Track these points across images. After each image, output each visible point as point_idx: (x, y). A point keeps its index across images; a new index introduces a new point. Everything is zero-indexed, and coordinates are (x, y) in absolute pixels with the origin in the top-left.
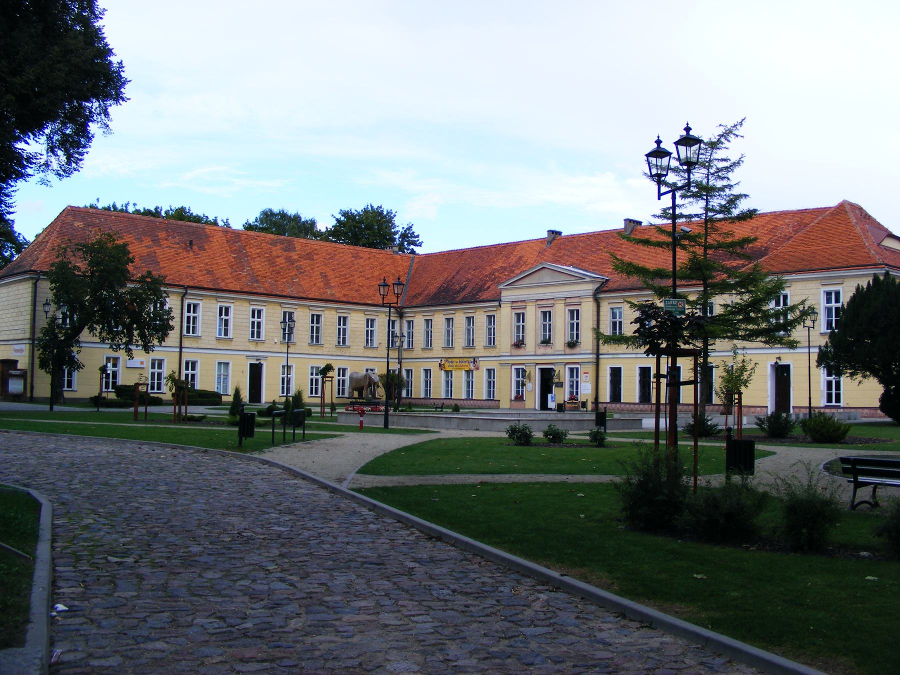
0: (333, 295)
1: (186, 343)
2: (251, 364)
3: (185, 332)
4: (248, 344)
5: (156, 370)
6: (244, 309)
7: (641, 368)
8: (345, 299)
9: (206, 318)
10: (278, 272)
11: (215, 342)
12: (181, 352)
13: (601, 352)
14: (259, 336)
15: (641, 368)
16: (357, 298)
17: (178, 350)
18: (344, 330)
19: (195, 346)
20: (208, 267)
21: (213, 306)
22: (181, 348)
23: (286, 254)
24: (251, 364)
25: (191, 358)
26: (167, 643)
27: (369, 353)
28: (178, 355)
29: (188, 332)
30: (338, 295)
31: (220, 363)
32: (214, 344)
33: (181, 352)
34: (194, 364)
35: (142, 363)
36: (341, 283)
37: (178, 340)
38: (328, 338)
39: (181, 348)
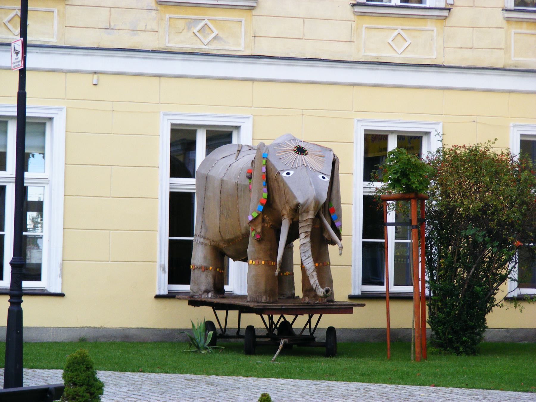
26: (373, 209)
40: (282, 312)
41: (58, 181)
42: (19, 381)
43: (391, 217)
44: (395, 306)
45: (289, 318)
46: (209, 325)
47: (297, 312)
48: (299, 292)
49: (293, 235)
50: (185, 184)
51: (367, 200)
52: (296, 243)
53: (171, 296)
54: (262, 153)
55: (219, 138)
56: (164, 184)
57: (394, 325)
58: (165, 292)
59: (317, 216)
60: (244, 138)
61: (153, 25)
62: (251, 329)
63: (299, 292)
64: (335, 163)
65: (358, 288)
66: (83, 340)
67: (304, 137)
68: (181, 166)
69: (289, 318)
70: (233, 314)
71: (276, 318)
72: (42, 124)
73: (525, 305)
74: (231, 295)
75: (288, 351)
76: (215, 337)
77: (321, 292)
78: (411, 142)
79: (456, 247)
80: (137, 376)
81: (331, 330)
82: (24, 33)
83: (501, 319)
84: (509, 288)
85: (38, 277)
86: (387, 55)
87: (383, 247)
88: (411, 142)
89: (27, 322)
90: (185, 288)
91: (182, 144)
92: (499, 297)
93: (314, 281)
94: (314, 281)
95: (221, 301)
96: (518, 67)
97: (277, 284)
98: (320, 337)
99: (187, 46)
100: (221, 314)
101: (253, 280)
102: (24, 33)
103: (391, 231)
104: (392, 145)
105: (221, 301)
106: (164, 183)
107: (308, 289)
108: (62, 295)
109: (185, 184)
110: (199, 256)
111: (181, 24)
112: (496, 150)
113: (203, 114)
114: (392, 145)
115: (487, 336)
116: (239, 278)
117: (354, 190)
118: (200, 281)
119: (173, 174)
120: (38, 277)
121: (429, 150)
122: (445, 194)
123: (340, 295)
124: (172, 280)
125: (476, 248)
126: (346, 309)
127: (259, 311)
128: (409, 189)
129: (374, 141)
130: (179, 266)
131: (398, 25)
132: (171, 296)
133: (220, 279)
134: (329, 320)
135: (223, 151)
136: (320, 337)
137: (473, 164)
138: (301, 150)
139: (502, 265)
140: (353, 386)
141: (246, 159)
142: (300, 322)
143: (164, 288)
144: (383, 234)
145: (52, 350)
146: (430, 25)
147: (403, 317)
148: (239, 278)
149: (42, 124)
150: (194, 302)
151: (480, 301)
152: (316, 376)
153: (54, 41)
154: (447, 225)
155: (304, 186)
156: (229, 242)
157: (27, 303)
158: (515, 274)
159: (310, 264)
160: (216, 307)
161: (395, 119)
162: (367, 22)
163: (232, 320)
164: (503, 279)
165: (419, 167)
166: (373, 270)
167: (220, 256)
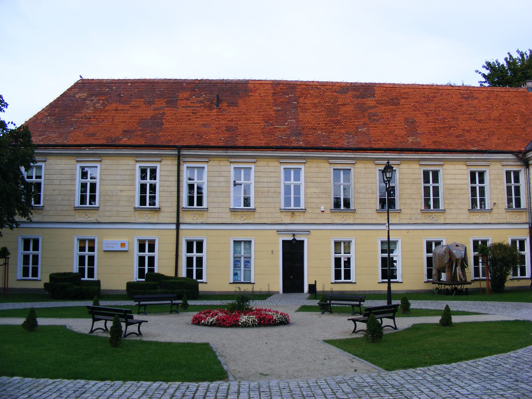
0: (418, 143)
1: (185, 218)
2: (284, 242)
3: (184, 203)
4: (279, 215)
5: (147, 254)
6: (272, 169)
7: (140, 241)
8: (433, 147)
9: (104, 177)
10: (338, 122)
11: (229, 215)
12: (178, 229)
13: (181, 221)
14: (200, 203)
15: (140, 241)
16: (455, 143)
17: (174, 227)
18: (436, 190)
19: (199, 221)
20: (230, 124)
21: (224, 169)
22: (178, 224)
23: (356, 101)
24: (284, 242)
25: (195, 237)
26: (476, 259)
27: (477, 218)
28: (175, 232)
29: (191, 203)
30: (424, 143)
31: (237, 243)
32: (228, 217)
33: (178, 229)
34: (200, 244)
35: (123, 245)
36: (435, 129)
37: (175, 215)
38: (409, 201)
39: (178, 224)
40: (455, 285)
41: (400, 255)
42: (391, 303)
43: (480, 261)
44: (482, 282)
45: (456, 286)
46: (437, 288)
47: (458, 285)
48: (458, 280)
49: (456, 266)
50: (430, 255)
51: (474, 257)
52: (457, 268)
53: (428, 282)
54: (448, 246)
55: (438, 243)
56: (425, 255)
57: (482, 287)
58: (333, 282)
59: (462, 262)
60: (444, 243)
61: (421, 217)
62: (447, 289)
63: (458, 280)
64: (466, 248)
65: (473, 278)
66: (407, 293)
67: (458, 242)
68: (429, 250)
69: (456, 286)
70: (443, 286)
71: (453, 286)
72: (395, 243)
73: (514, 281)
74: (442, 281)
75: (456, 294)
76: (439, 291)
77: (464, 279)
78: (484, 242)
79: (497, 267)
80: (420, 301)
81: (467, 289)
82: (388, 222)
83: (508, 284)
84: (510, 277)
85: (396, 278)
86: (477, 222)
87: (478, 268)
88: (484, 242)
89: (392, 289)
90: (431, 280)
91: (429, 245)
92: (508, 279)
93: (462, 277)
94: (462, 277)
95: (440, 282)
96: (156, 336)
97: (453, 279)
98: (464, 290)
99: (429, 222)
100: (440, 286)
101: (447, 277)
102: (388, 222)
103: (480, 264)
104: (480, 243)
105: (440, 282)
106: (425, 255)
107: (461, 279)
108: (206, 283)
109: (430, 255)
110: (434, 272)
111: (427, 217)
112: (505, 243)
113: (434, 238)
114: (480, 243)
115: (505, 288)
116: (444, 277)
117: (471, 254)
118: (435, 278)
119: (427, 252)
120: (396, 278)
121: (489, 244)
122: (493, 254)
123: (469, 280)
124: (428, 278)
125: (501, 268)
126: (470, 283)
127: (449, 285)
128: (484, 254)
129: (475, 242)
130: (430, 275)
131: (480, 214)
132: (428, 282)
133: (440, 277)
134: (466, 286)
135: (439, 246)
136: (464, 290)
137: (499, 247)
138: (457, 246)
139: (508, 271)
140: (472, 302)
141: (444, 248)
142: (459, 287)
143: (381, 280)
144: (479, 265)
145: (398, 295)
146: (487, 214)
147: (484, 285)
148: (444, 277)
149: (395, 243)
150: (434, 283)
151: (504, 280)
152: (463, 300)
153: (397, 223)
154: (494, 262)
155: (458, 254)
156: (441, 268)
157: (392, 285)
158: (511, 273)
159: (461, 273)
160: (439, 284)
161: (480, 237)
162: (472, 214)
163: (443, 287)
164: (508, 274)
165: (487, 248)
166: (477, 274)
167: (439, 272)
